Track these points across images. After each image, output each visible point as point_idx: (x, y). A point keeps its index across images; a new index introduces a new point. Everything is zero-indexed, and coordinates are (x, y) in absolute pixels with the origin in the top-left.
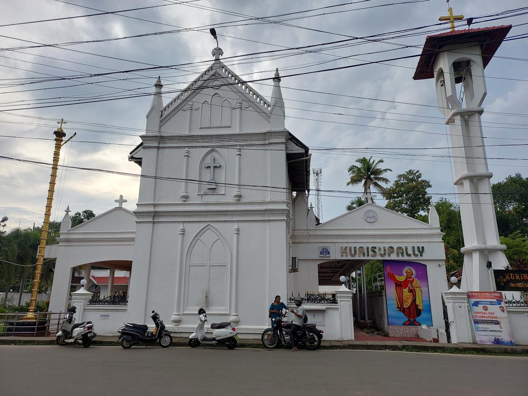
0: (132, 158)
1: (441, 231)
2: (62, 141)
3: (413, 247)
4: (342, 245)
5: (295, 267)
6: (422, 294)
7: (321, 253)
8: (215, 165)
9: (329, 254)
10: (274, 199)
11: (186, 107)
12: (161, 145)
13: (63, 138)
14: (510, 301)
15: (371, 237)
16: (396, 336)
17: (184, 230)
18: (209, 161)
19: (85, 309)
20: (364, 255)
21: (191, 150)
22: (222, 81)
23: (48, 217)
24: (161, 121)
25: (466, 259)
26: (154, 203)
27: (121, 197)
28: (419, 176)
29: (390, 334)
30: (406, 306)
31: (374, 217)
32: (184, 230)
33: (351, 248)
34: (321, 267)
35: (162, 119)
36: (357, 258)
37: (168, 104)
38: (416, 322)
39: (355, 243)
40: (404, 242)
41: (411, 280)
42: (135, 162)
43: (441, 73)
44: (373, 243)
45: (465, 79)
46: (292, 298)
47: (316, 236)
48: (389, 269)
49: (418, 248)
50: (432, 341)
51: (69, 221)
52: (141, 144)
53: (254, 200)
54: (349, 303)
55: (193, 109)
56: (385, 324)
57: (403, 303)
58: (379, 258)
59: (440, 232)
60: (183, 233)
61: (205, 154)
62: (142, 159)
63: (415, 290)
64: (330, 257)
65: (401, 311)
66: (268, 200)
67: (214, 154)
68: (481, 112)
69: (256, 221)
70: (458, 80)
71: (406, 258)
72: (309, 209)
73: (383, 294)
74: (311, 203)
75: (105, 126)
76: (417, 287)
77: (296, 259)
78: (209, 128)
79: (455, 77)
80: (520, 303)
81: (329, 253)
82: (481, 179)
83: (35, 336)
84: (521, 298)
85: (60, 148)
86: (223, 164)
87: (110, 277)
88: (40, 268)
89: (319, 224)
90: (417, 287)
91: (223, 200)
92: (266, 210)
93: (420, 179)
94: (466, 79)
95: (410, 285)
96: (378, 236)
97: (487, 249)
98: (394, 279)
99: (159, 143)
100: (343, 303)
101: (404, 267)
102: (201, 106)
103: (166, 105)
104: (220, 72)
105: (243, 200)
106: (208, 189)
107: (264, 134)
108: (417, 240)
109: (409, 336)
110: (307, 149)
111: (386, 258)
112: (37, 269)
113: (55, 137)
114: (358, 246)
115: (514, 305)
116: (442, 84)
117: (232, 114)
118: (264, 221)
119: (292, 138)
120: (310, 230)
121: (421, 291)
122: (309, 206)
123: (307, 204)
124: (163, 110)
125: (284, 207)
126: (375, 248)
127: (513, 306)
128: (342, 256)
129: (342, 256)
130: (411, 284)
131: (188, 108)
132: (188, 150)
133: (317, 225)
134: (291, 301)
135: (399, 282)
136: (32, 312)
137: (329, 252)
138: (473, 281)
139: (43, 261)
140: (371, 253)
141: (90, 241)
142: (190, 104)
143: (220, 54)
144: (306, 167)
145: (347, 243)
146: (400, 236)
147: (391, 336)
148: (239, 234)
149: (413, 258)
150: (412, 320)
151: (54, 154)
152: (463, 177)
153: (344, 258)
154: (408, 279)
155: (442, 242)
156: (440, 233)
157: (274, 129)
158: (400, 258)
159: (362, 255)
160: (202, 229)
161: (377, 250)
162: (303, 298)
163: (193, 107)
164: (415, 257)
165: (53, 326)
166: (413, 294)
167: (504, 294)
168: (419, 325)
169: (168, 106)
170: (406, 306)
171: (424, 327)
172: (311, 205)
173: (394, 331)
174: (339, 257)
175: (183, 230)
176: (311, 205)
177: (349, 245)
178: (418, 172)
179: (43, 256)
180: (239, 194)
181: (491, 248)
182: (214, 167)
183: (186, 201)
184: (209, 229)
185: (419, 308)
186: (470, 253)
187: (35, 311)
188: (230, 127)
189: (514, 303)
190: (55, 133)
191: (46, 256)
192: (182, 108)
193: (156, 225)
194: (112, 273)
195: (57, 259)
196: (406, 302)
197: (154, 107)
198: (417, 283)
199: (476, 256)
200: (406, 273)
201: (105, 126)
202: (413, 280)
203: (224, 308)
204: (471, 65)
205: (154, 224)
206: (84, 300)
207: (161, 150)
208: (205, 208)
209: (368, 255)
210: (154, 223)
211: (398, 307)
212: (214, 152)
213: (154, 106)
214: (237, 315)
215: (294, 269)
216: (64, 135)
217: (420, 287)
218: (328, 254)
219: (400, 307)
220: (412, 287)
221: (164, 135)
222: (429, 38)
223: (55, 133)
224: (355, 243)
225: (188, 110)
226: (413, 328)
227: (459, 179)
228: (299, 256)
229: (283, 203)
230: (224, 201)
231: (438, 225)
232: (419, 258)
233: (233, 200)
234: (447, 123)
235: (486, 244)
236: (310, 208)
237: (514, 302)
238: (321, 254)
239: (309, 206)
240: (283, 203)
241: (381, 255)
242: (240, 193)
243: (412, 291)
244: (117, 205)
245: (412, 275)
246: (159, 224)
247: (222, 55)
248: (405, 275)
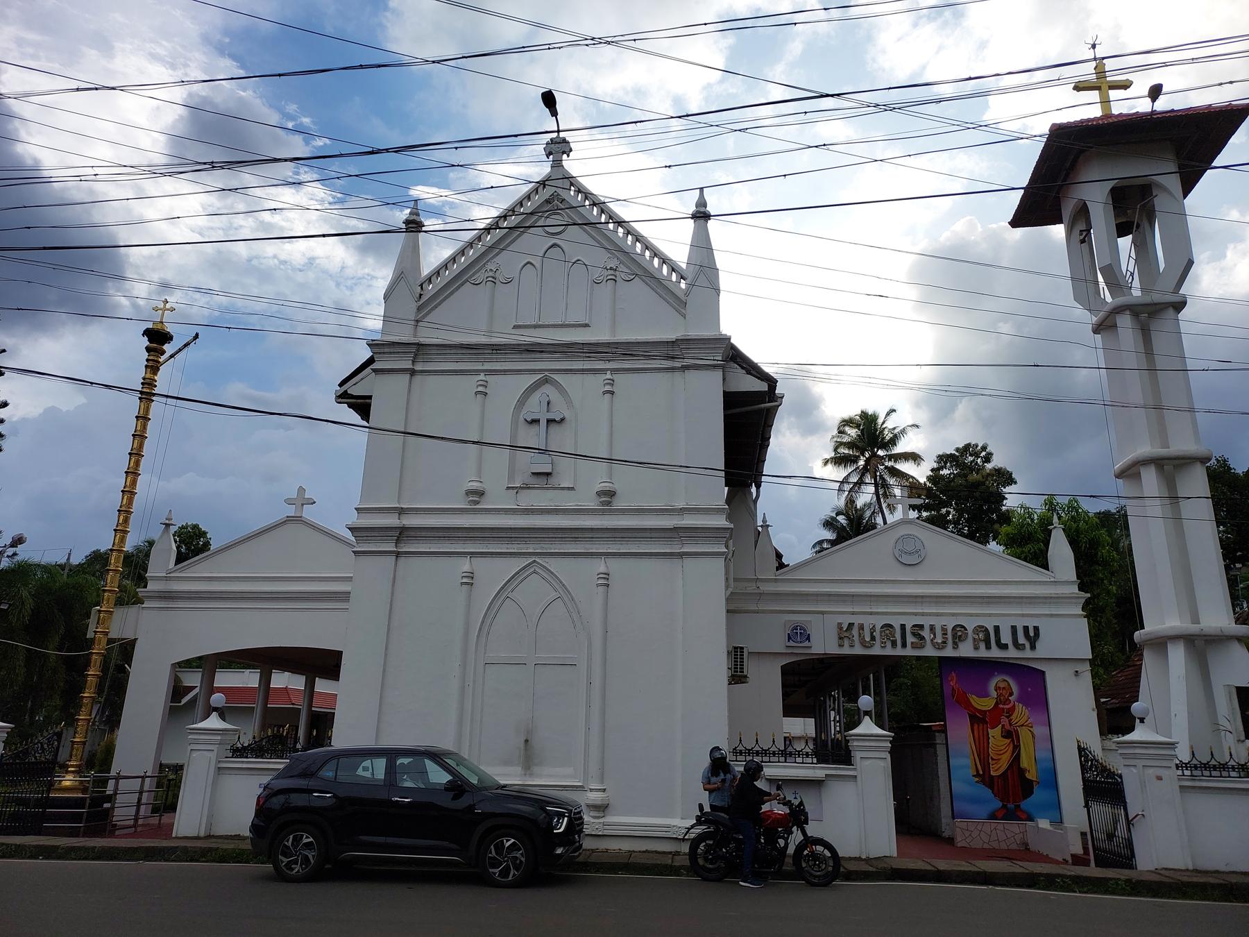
0: (343, 397)
1: (1079, 590)
2: (163, 352)
3: (1014, 629)
4: (840, 619)
5: (740, 672)
6: (1034, 742)
7: (789, 638)
8: (551, 416)
9: (809, 641)
10: (693, 504)
11: (481, 276)
12: (419, 367)
13: (166, 347)
14: (1222, 764)
15: (911, 599)
16: (974, 845)
17: (471, 575)
18: (535, 407)
19: (219, 768)
20: (894, 644)
21: (491, 379)
22: (569, 217)
23: (124, 537)
24: (419, 309)
25: (1149, 662)
26: (398, 506)
27: (301, 490)
28: (988, 459)
29: (959, 839)
30: (996, 770)
31: (917, 552)
32: (471, 575)
33: (861, 627)
34: (786, 671)
35: (421, 303)
36: (876, 651)
37: (437, 267)
38: (1021, 810)
39: (871, 613)
40: (990, 615)
41: (1007, 707)
42: (350, 406)
43: (1083, 212)
44: (916, 614)
45: (1138, 226)
46: (740, 748)
47: (778, 596)
48: (954, 681)
49: (1026, 629)
50: (1070, 861)
51: (172, 548)
52: (370, 361)
53: (645, 505)
54: (882, 763)
55: (497, 281)
56: (942, 815)
57: (989, 764)
58: (929, 651)
59: (1077, 591)
60: (469, 580)
61: (526, 390)
62: (370, 397)
63: (1017, 732)
64: (811, 647)
65: (984, 784)
66: (680, 504)
67: (547, 389)
68: (1180, 305)
69: (651, 554)
70: (1122, 231)
71: (995, 653)
72: (760, 529)
73: (938, 742)
74: (764, 514)
75: (322, 309)
76: (1022, 725)
77: (743, 652)
78: (536, 327)
79: (1117, 222)
80: (1229, 768)
81: (808, 638)
82: (1186, 464)
83: (81, 835)
84: (1211, 756)
85: (159, 369)
86: (567, 414)
87: (260, 690)
88: (98, 664)
89: (781, 566)
90: (1022, 725)
91: (569, 501)
92: (676, 529)
93: (989, 466)
94: (1141, 227)
95: (1004, 720)
96: (928, 599)
97: (1205, 636)
98: (968, 705)
99: (413, 362)
100: (868, 762)
101: (990, 676)
102: (518, 275)
103: (1160, 181)
104: (563, 194)
105: (619, 503)
106: (533, 473)
107: (673, 343)
108: (853, 608)
109: (1003, 846)
110: (772, 382)
111: (949, 652)
112: (92, 664)
113: (145, 342)
114: (879, 622)
115: (1214, 773)
116: (1082, 237)
117: (591, 294)
118: (671, 554)
119: (735, 358)
120: (762, 580)
121: (1033, 736)
122: (760, 523)
123: (754, 515)
124: (425, 282)
125: (721, 521)
126: (921, 627)
127: (1213, 775)
128: (840, 645)
129: (841, 646)
130: (1008, 717)
131: (487, 278)
132: (484, 379)
133: (778, 569)
134: (736, 756)
135: (980, 711)
136: (73, 772)
137: (809, 634)
138: (1173, 715)
139: (107, 645)
140: (910, 639)
141: (190, 598)
142: (491, 270)
143: (564, 153)
144: (764, 426)
145: (853, 613)
146: (980, 600)
147: (959, 845)
148: (608, 585)
149: (1012, 653)
150: (1011, 806)
151: (142, 384)
152: (1140, 459)
153: (846, 651)
154: (1001, 706)
155: (1082, 615)
156: (1077, 594)
157: (694, 333)
158: (983, 653)
159: (889, 644)
160: (517, 573)
161: (926, 633)
162: (768, 750)
163: (497, 275)
164: (999, 649)
165: (123, 812)
166: (1014, 743)
167: (1228, 748)
168: (1030, 818)
169: (437, 273)
170: (996, 770)
171: (1044, 824)
172: (764, 521)
173: (967, 834)
174: (832, 648)
175: (471, 575)
176: (764, 521)
177: (857, 620)
178: (984, 448)
179: (106, 634)
180: (610, 487)
181: (1213, 633)
182: (549, 421)
183: (478, 503)
184: (535, 572)
185: (1028, 776)
186: (1161, 643)
187: (78, 772)
188: (587, 325)
189: (1215, 768)
190: (147, 333)
191: (112, 635)
192: (471, 277)
193: (402, 560)
194: (266, 680)
195: (138, 642)
196: (996, 761)
197: (402, 275)
198: (1023, 713)
199: (1177, 656)
200: (996, 690)
201: (322, 309)
202: (1013, 708)
203: (570, 770)
204: (1154, 194)
205: (397, 557)
206: (217, 746)
207: (418, 378)
208: (524, 520)
209: (904, 645)
210: (398, 555)
211: (977, 775)
212: (547, 386)
213: (402, 272)
214: (604, 790)
215: (737, 677)
216: (167, 338)
217: (1030, 725)
218: (807, 639)
219: (981, 772)
220: (1010, 725)
221: (428, 341)
222: (1056, 130)
223: (147, 333)
224: (871, 613)
225: (484, 282)
226: (1014, 827)
227: (1130, 463)
228: (750, 646)
229: (718, 511)
230: (571, 505)
231: (1073, 576)
232: (1028, 653)
233: (592, 504)
234: (1096, 330)
235: (1199, 624)
236: (762, 526)
237: (1214, 766)
238: (789, 641)
239: (760, 523)
240: (718, 511)
241: (864, 644)
242: (611, 485)
243: (1010, 735)
244: (291, 511)
245: (1011, 694)
246: (411, 559)
247: (568, 156)
248: (994, 694)
